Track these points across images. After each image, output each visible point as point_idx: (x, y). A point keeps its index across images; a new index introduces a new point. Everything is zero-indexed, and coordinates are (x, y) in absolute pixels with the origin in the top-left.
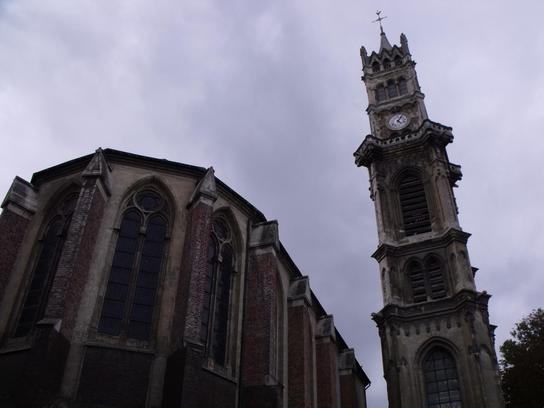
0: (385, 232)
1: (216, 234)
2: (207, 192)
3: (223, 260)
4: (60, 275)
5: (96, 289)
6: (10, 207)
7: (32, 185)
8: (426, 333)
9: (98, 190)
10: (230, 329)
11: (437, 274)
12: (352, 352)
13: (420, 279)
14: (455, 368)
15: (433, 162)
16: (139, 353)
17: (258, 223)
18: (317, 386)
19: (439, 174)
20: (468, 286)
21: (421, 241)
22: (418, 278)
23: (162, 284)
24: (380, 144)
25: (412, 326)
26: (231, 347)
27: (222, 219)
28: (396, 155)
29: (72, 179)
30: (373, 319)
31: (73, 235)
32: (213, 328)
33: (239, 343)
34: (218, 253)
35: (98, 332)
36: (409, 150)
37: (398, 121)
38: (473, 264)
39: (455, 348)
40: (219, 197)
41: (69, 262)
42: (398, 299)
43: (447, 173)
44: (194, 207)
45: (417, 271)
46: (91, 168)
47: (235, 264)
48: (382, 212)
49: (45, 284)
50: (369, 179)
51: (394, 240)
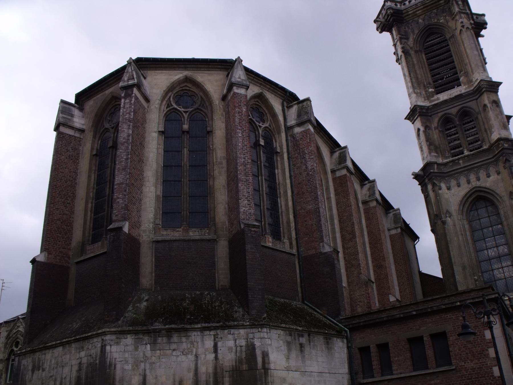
0: (415, 93)
1: (254, 120)
2: (239, 82)
3: (265, 143)
4: (119, 182)
5: (153, 189)
6: (62, 129)
7: (76, 105)
8: (466, 185)
9: (137, 98)
10: (281, 206)
11: (471, 127)
12: (398, 211)
13: (455, 134)
14: (498, 214)
15: (456, 15)
16: (202, 240)
17: (292, 103)
18: (370, 247)
19: (463, 26)
20: (504, 134)
21: (452, 97)
22: (453, 133)
23: (212, 174)
24: (399, 6)
25: (452, 180)
26: (285, 222)
27: (257, 105)
28: (416, 15)
29: (111, 93)
30: (414, 178)
31: (122, 144)
32: (265, 207)
33: (291, 217)
34: (259, 138)
35: (162, 227)
36: (429, 7)
38: (507, 112)
39: (496, 196)
40: (251, 84)
41: (124, 169)
42: (435, 156)
43: (471, 24)
44: (229, 98)
45: (451, 126)
46: (126, 79)
47: (276, 145)
48: (410, 74)
49: (107, 193)
50: (393, 44)
51: (425, 100)
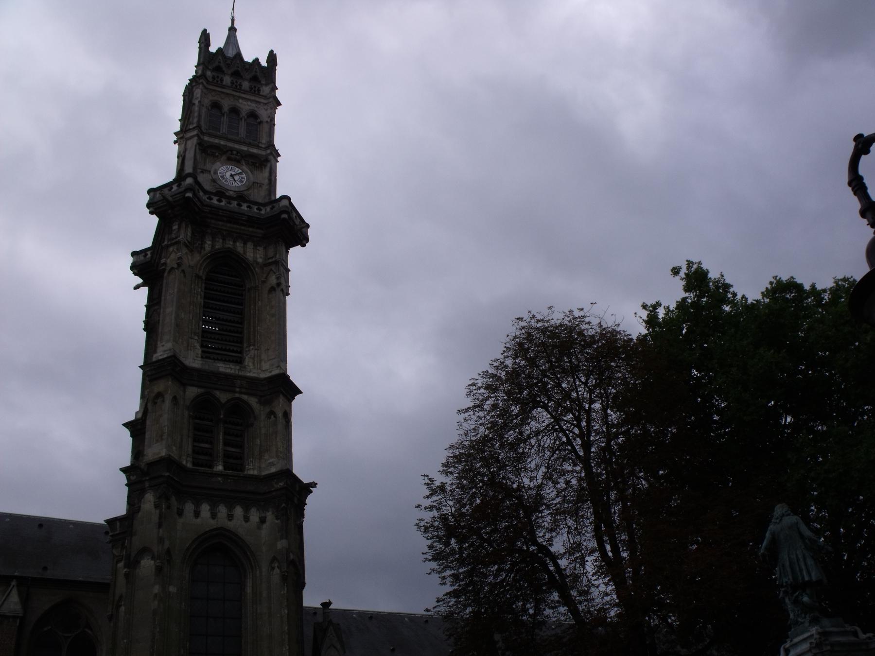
37: (232, 176)
